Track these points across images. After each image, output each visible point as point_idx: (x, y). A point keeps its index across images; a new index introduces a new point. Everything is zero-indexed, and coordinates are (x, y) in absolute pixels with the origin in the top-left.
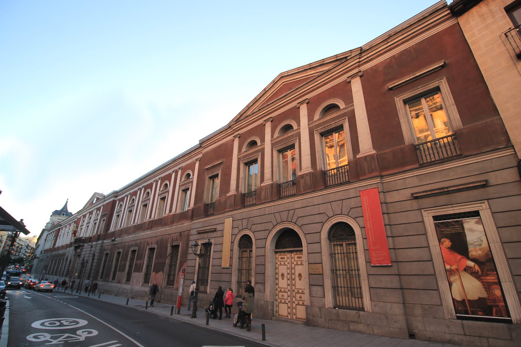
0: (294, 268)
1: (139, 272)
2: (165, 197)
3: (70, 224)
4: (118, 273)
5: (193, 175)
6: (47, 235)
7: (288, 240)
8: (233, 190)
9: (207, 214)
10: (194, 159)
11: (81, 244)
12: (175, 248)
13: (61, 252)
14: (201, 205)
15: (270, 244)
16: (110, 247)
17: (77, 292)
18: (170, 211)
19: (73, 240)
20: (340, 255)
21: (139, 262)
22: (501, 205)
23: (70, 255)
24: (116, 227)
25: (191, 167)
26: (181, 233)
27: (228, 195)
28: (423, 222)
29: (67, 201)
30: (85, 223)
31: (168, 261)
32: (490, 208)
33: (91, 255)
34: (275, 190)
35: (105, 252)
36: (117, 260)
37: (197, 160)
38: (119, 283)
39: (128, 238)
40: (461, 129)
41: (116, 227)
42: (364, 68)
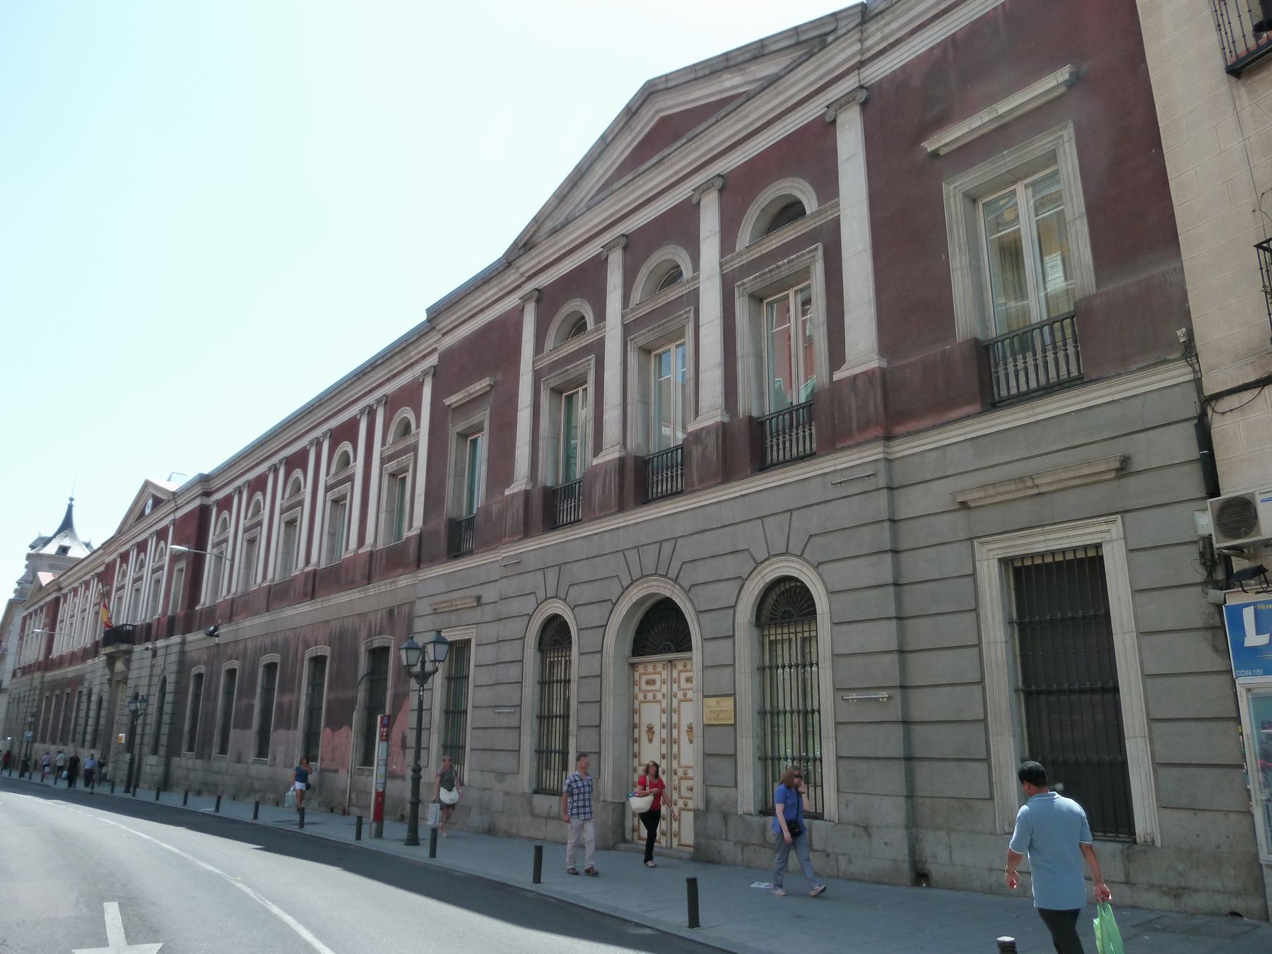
0: (678, 711)
1: (288, 728)
2: (344, 497)
3: (87, 584)
4: (234, 733)
5: (418, 426)
6: (25, 619)
7: (660, 630)
8: (520, 483)
9: (455, 551)
10: (417, 370)
11: (124, 647)
12: (379, 655)
13: (70, 671)
14: (440, 524)
15: (615, 640)
16: (205, 657)
17: (127, 791)
18: (308, 561)
19: (100, 636)
20: (787, 670)
21: (245, 701)
22: (1154, 526)
23: (97, 681)
24: (216, 590)
25: (410, 395)
26: (391, 612)
27: (508, 492)
28: (973, 575)
29: (70, 507)
30: (147, 572)
31: (361, 695)
32: (1125, 538)
33: (156, 680)
34: (630, 478)
35: (194, 671)
36: (229, 693)
37: (425, 373)
38: (238, 761)
39: (252, 626)
40: (1088, 298)
41: (216, 590)
42: (877, 71)
